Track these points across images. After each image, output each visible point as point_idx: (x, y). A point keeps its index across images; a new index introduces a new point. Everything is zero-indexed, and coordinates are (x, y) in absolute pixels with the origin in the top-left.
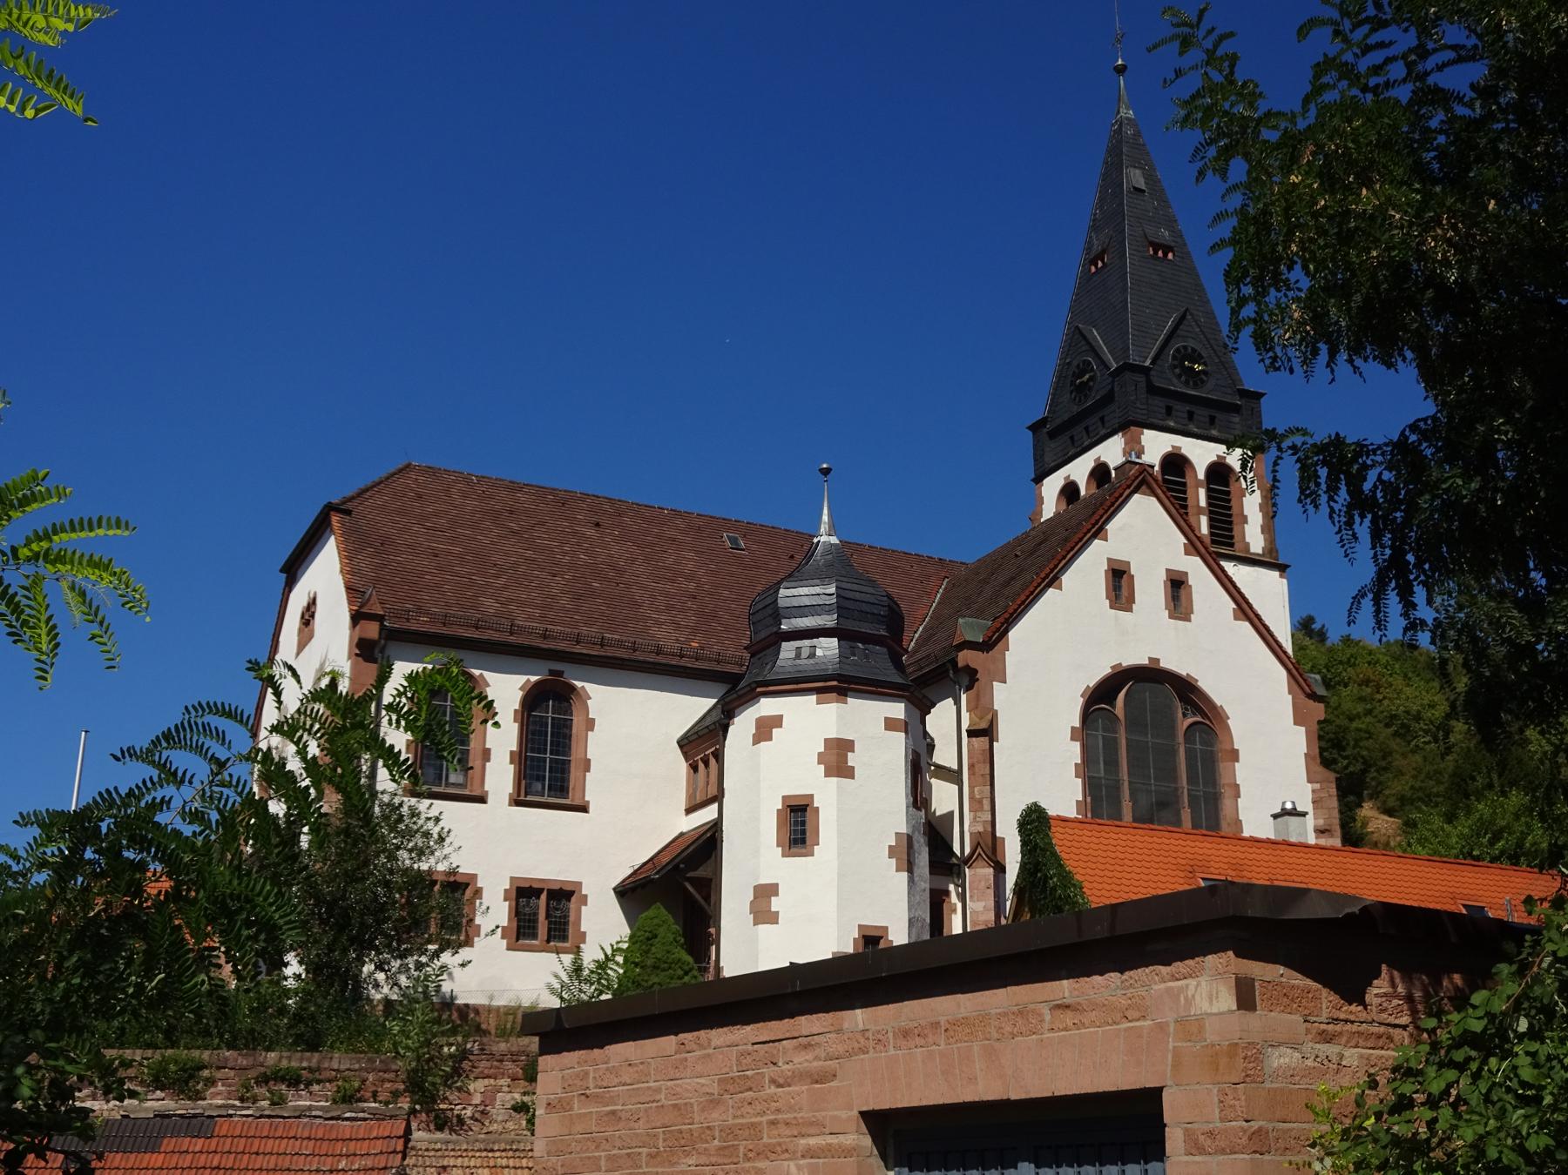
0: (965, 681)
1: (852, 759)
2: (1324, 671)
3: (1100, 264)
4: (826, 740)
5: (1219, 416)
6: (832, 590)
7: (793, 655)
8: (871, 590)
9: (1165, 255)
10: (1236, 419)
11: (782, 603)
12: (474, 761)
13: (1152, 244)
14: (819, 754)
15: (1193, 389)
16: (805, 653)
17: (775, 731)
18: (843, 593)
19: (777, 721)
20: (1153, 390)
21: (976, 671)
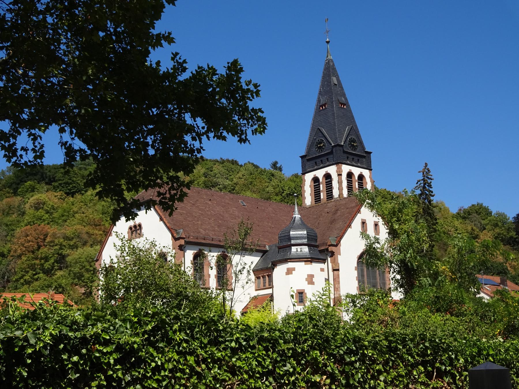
0: (330, 254)
1: (314, 280)
2: (294, 189)
3: (324, 107)
4: (308, 275)
5: (360, 159)
6: (305, 232)
7: (295, 250)
8: (312, 232)
9: (344, 106)
10: (364, 160)
11: (291, 236)
12: (206, 278)
13: (341, 103)
14: (306, 279)
15: (354, 151)
16: (299, 250)
17: (293, 272)
18: (309, 234)
19: (294, 269)
20: (345, 152)
21: (334, 252)
